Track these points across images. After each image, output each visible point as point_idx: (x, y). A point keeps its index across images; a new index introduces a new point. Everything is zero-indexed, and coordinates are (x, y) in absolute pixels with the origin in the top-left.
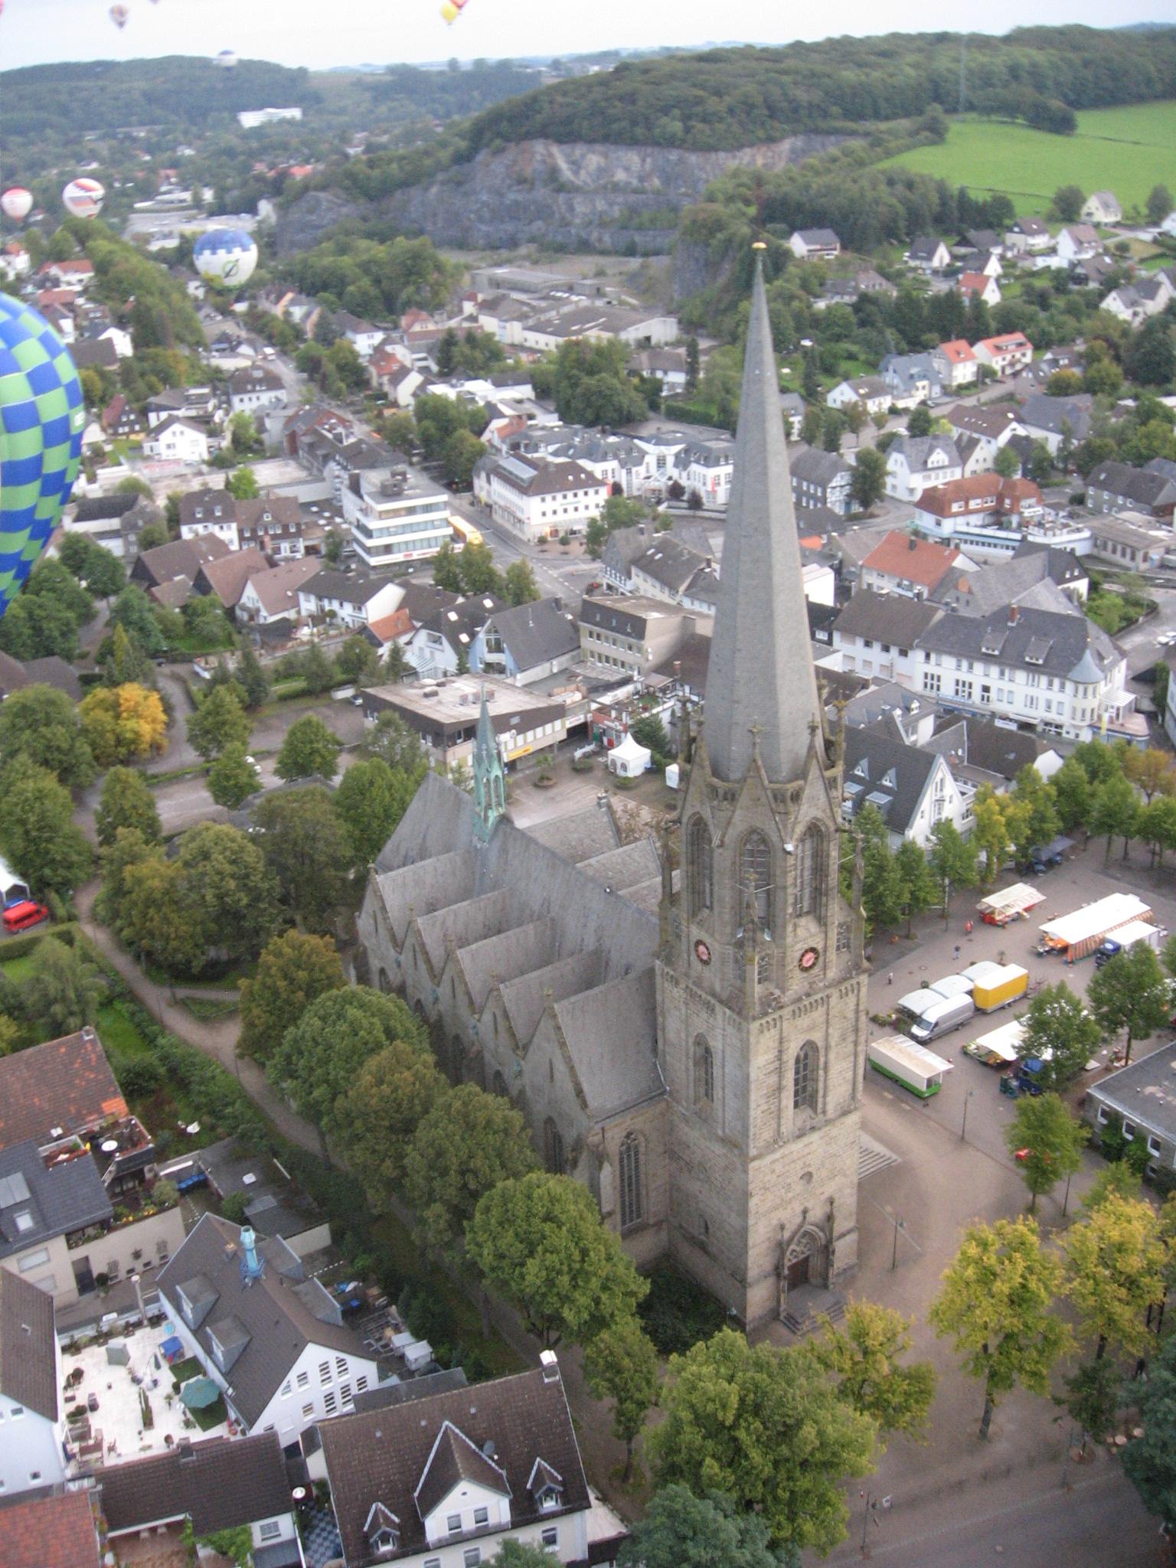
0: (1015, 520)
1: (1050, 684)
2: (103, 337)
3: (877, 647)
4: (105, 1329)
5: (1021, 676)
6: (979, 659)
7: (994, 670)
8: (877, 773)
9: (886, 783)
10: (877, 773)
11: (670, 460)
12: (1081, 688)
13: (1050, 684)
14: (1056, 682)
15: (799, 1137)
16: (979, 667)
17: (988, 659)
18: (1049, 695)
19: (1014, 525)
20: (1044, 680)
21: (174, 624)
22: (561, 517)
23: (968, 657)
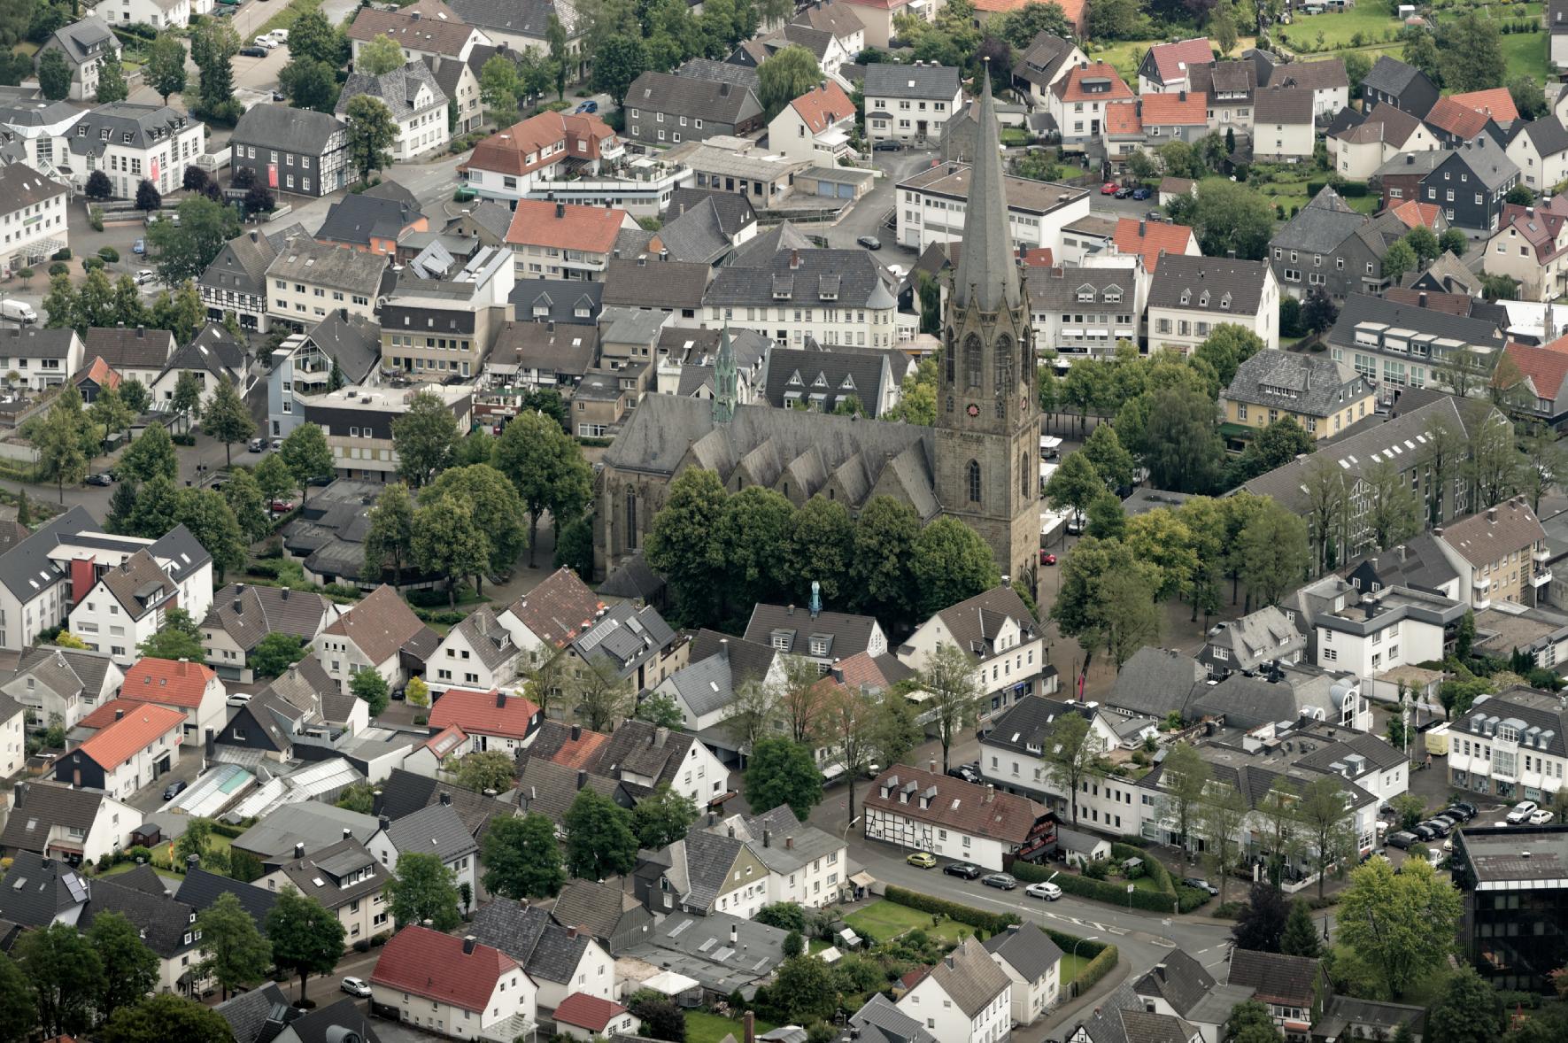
0: (596, 165)
1: (849, 317)
2: (1404, 769)
3: (329, 293)
4: (591, 494)
5: (818, 314)
6: (772, 306)
7: (790, 314)
8: (809, 379)
9: (794, 382)
10: (809, 379)
11: (59, 145)
12: (881, 315)
13: (849, 317)
14: (803, 314)
15: (661, 436)
16: (773, 314)
17: (781, 304)
18: (849, 327)
19: (595, 174)
20: (842, 314)
21: (795, 482)
22: (25, 241)
23: (725, 305)
